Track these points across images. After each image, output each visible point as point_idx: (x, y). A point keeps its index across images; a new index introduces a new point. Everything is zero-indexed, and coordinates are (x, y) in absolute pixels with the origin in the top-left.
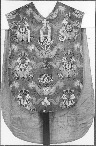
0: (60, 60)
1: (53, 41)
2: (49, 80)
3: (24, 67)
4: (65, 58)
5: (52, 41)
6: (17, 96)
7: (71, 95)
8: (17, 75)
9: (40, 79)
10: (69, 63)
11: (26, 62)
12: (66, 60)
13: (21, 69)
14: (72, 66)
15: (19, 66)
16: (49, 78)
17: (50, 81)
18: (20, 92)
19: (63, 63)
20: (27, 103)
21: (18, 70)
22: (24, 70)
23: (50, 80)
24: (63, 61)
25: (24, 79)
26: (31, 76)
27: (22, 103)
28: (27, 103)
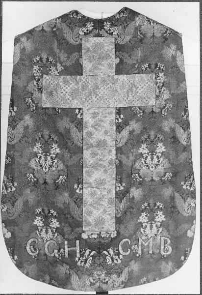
0: (30, 148)
1: (15, 110)
2: (7, 189)
3: (47, 162)
4: (38, 145)
5: (13, 109)
6: (138, 218)
7: (157, 212)
8: (140, 177)
9: (78, 187)
10: (46, 155)
11: (158, 150)
12: (40, 149)
13: (147, 166)
14: (159, 160)
15: (37, 160)
16: (8, 184)
17: (9, 191)
18: (40, 212)
19: (36, 154)
20: (158, 231)
21: (35, 167)
22: (47, 167)
23: (10, 189)
24: (35, 150)
25: (47, 186)
26: (62, 181)
27: (148, 232)
28: (158, 231)
